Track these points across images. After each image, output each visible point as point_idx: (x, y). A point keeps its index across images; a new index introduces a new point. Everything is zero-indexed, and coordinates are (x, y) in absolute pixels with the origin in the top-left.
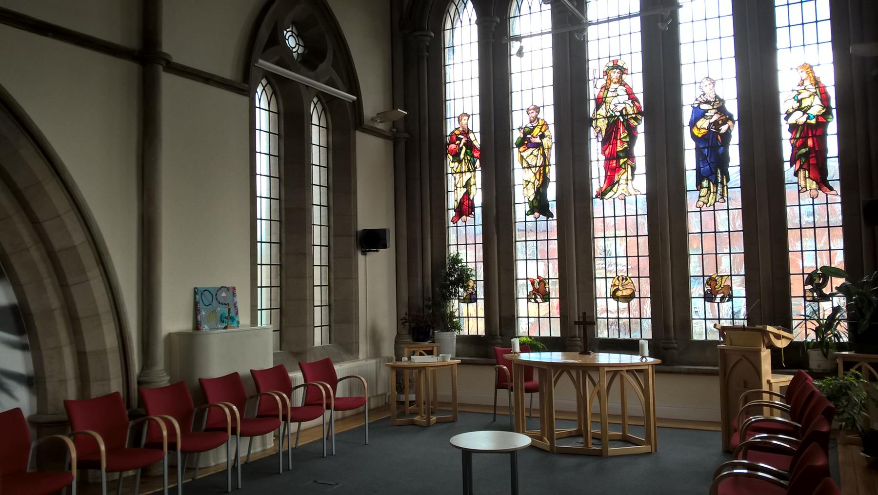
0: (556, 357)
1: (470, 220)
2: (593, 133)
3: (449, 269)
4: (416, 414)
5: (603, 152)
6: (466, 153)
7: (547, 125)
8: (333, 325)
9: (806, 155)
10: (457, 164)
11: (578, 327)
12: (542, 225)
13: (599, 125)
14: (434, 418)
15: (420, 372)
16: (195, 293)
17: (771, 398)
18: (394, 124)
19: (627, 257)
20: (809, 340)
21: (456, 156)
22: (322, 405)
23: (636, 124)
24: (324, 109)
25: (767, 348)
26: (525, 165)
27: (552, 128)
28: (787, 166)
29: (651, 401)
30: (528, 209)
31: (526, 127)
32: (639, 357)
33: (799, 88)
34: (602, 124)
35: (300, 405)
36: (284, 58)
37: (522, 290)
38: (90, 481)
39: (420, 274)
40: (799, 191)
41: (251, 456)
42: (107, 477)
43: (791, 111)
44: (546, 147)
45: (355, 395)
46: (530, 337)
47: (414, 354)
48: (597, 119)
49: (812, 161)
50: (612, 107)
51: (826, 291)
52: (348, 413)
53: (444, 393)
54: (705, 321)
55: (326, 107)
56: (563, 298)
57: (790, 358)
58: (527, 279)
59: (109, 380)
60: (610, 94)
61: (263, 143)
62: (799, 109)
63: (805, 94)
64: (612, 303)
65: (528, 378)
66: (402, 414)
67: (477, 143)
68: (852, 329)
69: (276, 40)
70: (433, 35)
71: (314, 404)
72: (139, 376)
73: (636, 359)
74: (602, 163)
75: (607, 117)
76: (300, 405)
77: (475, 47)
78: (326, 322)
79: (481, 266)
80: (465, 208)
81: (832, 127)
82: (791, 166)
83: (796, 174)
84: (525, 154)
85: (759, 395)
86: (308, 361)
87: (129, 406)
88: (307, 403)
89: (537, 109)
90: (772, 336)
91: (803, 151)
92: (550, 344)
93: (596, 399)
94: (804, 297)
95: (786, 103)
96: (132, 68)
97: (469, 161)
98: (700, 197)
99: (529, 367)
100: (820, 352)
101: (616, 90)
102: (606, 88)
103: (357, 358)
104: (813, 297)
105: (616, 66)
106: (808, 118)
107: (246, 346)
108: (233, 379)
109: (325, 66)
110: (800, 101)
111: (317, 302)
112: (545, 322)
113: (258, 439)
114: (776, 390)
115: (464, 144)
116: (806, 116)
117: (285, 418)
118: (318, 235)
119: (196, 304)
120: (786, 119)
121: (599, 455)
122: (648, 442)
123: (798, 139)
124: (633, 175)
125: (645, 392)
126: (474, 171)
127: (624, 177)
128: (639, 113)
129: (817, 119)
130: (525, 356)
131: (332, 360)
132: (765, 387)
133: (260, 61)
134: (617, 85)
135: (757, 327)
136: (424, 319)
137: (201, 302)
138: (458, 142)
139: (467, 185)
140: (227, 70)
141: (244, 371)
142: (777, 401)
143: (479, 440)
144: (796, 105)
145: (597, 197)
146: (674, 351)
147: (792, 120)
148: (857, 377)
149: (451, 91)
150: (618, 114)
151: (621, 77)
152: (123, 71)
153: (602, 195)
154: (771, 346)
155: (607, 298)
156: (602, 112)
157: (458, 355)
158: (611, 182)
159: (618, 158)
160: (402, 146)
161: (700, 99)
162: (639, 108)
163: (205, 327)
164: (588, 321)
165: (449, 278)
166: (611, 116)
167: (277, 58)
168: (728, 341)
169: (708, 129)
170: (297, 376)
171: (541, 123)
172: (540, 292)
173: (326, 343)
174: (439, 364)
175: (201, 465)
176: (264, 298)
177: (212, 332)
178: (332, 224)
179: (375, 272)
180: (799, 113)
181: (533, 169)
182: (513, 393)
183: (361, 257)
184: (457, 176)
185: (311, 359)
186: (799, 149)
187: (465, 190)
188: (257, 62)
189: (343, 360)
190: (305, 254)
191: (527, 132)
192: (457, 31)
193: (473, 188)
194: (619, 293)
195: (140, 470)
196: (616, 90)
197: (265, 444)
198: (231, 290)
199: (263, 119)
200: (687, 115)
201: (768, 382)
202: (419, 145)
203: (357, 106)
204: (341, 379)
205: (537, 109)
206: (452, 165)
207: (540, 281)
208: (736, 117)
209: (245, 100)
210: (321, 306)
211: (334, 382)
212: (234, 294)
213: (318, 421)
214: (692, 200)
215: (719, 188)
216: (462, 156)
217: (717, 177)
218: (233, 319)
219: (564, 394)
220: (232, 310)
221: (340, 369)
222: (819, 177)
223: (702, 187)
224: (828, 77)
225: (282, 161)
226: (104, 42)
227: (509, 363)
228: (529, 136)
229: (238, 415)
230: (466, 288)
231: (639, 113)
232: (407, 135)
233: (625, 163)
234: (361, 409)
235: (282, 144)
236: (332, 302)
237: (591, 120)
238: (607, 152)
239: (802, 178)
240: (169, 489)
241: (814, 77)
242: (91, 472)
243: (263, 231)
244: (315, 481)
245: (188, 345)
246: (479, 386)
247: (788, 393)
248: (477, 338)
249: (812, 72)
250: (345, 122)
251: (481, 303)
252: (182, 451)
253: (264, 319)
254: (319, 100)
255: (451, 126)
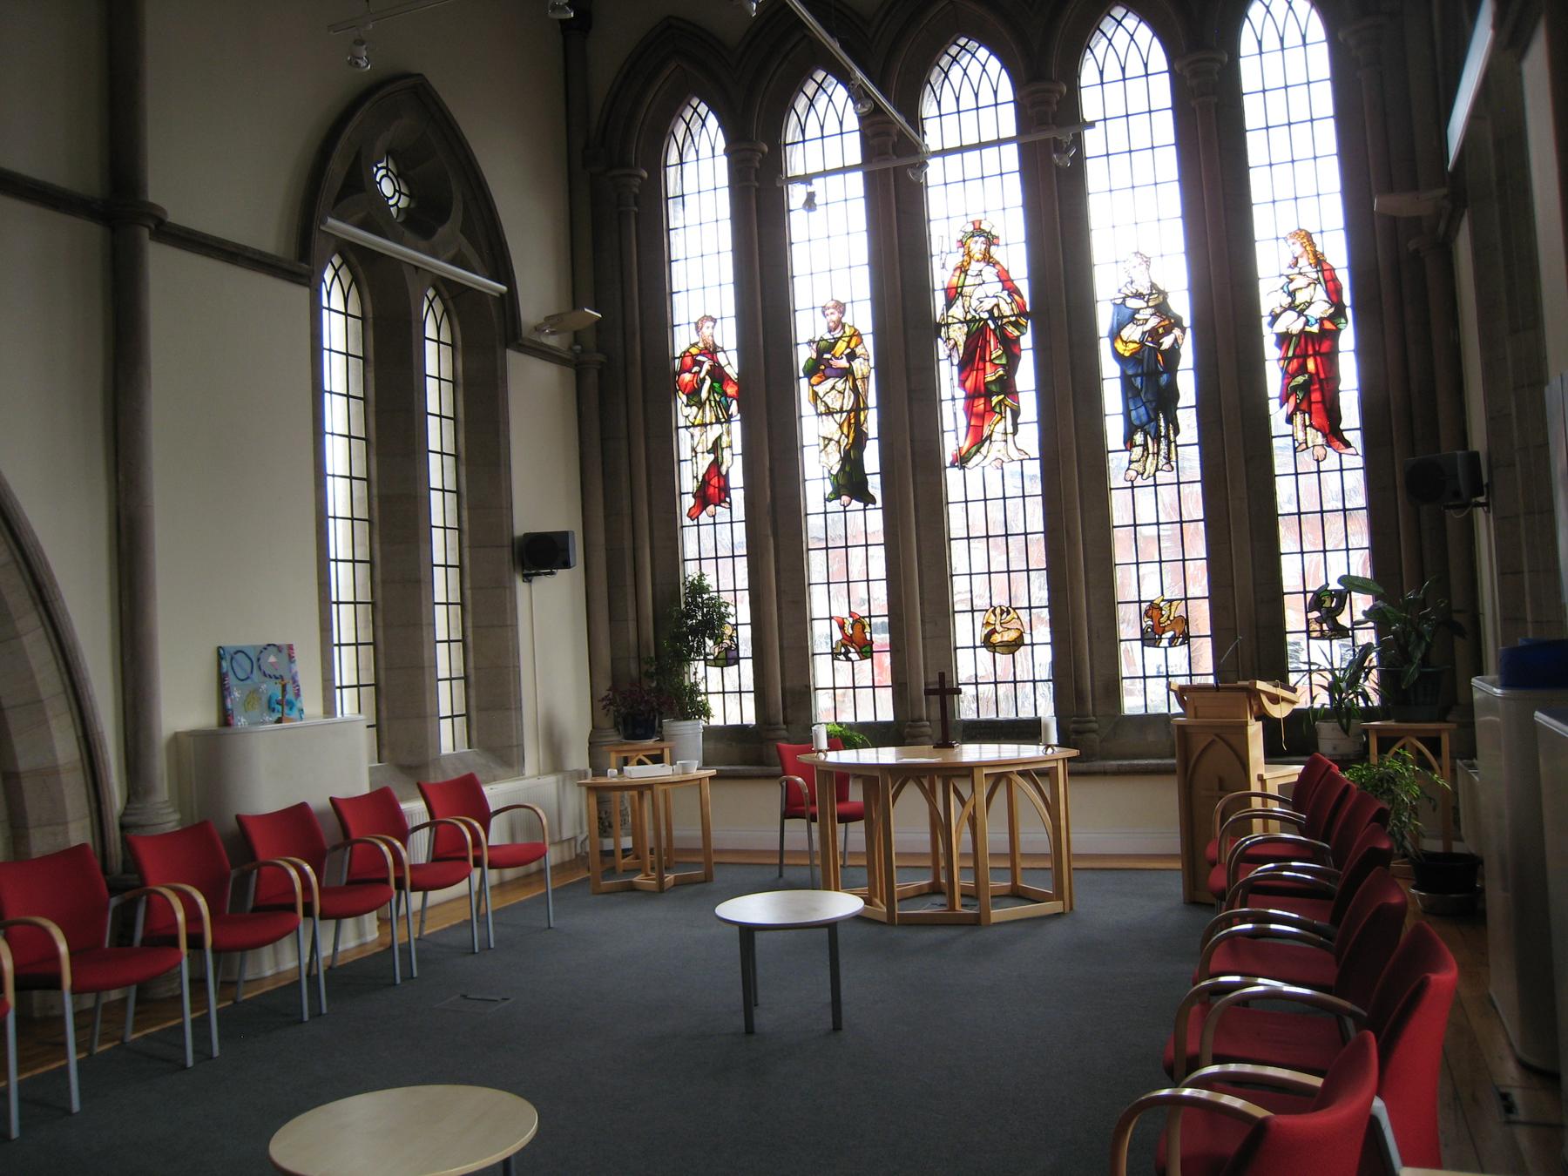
0: (888, 755)
1: (722, 513)
2: (942, 349)
3: (687, 604)
4: (637, 871)
5: (962, 384)
6: (712, 387)
7: (859, 335)
8: (473, 714)
9: (1305, 387)
10: (695, 409)
11: (926, 703)
12: (856, 519)
13: (952, 334)
14: (670, 878)
15: (641, 795)
16: (220, 658)
17: (1264, 804)
18: (577, 337)
19: (1009, 572)
20: (1317, 705)
21: (693, 394)
22: (466, 859)
23: (1016, 333)
24: (446, 310)
25: (1257, 719)
26: (822, 409)
27: (869, 341)
28: (1274, 406)
29: (1063, 823)
30: (829, 489)
31: (822, 339)
32: (1042, 748)
33: (1290, 271)
34: (958, 334)
35: (423, 861)
36: (375, 217)
37: (822, 635)
38: (37, 1014)
39: (631, 614)
40: (1295, 449)
41: (339, 957)
42: (74, 1005)
43: (1278, 311)
44: (858, 375)
45: (521, 840)
46: (840, 724)
47: (626, 762)
48: (948, 325)
49: (1315, 399)
50: (975, 303)
51: (1344, 620)
52: (510, 873)
53: (686, 831)
54: (1151, 680)
55: (451, 306)
56: (896, 649)
57: (1290, 738)
58: (831, 618)
59: (66, 823)
60: (970, 281)
61: (336, 373)
62: (1292, 307)
63: (1300, 282)
64: (984, 655)
65: (843, 796)
66: (611, 871)
67: (732, 371)
68: (1388, 683)
69: (358, 183)
70: (645, 175)
71: (451, 858)
72: (124, 814)
73: (1030, 751)
74: (960, 404)
75: (966, 322)
76: (423, 861)
77: (724, 196)
78: (460, 708)
79: (744, 597)
80: (712, 491)
81: (1347, 339)
82: (1282, 406)
83: (1290, 420)
84: (821, 390)
85: (1246, 800)
86: (432, 781)
87: (105, 871)
88: (437, 856)
89: (840, 307)
90: (1264, 698)
91: (1300, 379)
92: (875, 734)
93: (967, 829)
94: (1308, 632)
95: (1270, 298)
96: (91, 233)
97: (718, 403)
98: (1131, 462)
99: (843, 775)
100: (1337, 725)
101: (980, 274)
102: (963, 269)
103: (521, 774)
104: (1322, 631)
105: (978, 231)
106: (1307, 323)
107: (318, 754)
108: (300, 813)
109: (449, 230)
110: (1292, 294)
111: (443, 672)
112: (865, 696)
113: (349, 924)
114: (1272, 789)
115: (708, 373)
116: (1303, 319)
117: (400, 885)
118: (442, 546)
119: (222, 678)
120: (1272, 324)
121: (976, 922)
122: (1059, 895)
123: (1290, 360)
124: (1015, 425)
125: (1052, 807)
126: (728, 420)
127: (1000, 428)
128: (1022, 314)
129: (1321, 324)
130: (833, 757)
131: (479, 777)
132: (1255, 787)
133: (331, 221)
134: (982, 264)
135: (1240, 683)
136: (640, 697)
137: (231, 673)
138: (696, 369)
139: (716, 448)
140: (269, 237)
141: (318, 801)
142: (1275, 807)
143: (753, 908)
144: (1287, 300)
145: (953, 465)
146: (1093, 736)
147: (1280, 327)
148: (1404, 762)
149: (681, 276)
150: (985, 316)
151: (987, 251)
152: (82, 237)
153: (962, 461)
154: (1263, 716)
155: (975, 647)
156: (957, 311)
157: (706, 764)
158: (979, 440)
159: (988, 395)
160: (592, 378)
161: (1125, 291)
162: (1021, 306)
163: (241, 721)
164: (946, 690)
165: (687, 623)
166: (974, 320)
167: (361, 215)
168: (1192, 712)
169: (1142, 343)
170: (415, 809)
171: (848, 331)
172: (855, 643)
173: (463, 748)
174: (676, 779)
175: (249, 976)
176: (346, 666)
177: (254, 728)
178: (466, 526)
179: (550, 612)
180: (1292, 315)
181: (837, 417)
182: (815, 826)
183: (521, 587)
184: (697, 431)
185: (435, 777)
186: (1294, 377)
187: (712, 457)
188: (324, 222)
189: (495, 779)
190: (418, 581)
191: (824, 349)
192: (689, 169)
193: (727, 454)
194: (996, 638)
195: (133, 989)
196: (980, 274)
197: (359, 934)
198: (285, 651)
199: (335, 330)
200: (1104, 319)
201: (1261, 778)
202: (623, 377)
203: (509, 302)
204: (498, 812)
205: (840, 307)
206: (687, 411)
207: (855, 621)
208: (1187, 322)
209: (304, 293)
210: (451, 679)
211: (485, 817)
212: (291, 658)
213: (461, 888)
214: (1118, 464)
215: (1163, 446)
216: (704, 395)
217: (1158, 426)
218: (291, 705)
219: (909, 820)
220: (290, 688)
221: (495, 793)
222: (1326, 423)
223: (1133, 445)
224: (1337, 254)
225: (372, 409)
226: (35, 182)
227: (807, 771)
228: (827, 356)
229: (313, 879)
230: (718, 639)
231: (1022, 314)
232: (600, 357)
233: (1000, 402)
234: (534, 866)
235: (371, 376)
236: (471, 672)
237: (939, 326)
238: (968, 384)
239: (1300, 427)
240: (193, 1021)
241: (1315, 253)
242: (37, 996)
243: (340, 539)
244: (464, 996)
245: (210, 753)
246: (751, 816)
247: (1297, 795)
248: (741, 729)
249: (1312, 244)
250: (488, 333)
251: (747, 666)
252: (215, 950)
253: (347, 703)
254: (438, 293)
255: (683, 340)
